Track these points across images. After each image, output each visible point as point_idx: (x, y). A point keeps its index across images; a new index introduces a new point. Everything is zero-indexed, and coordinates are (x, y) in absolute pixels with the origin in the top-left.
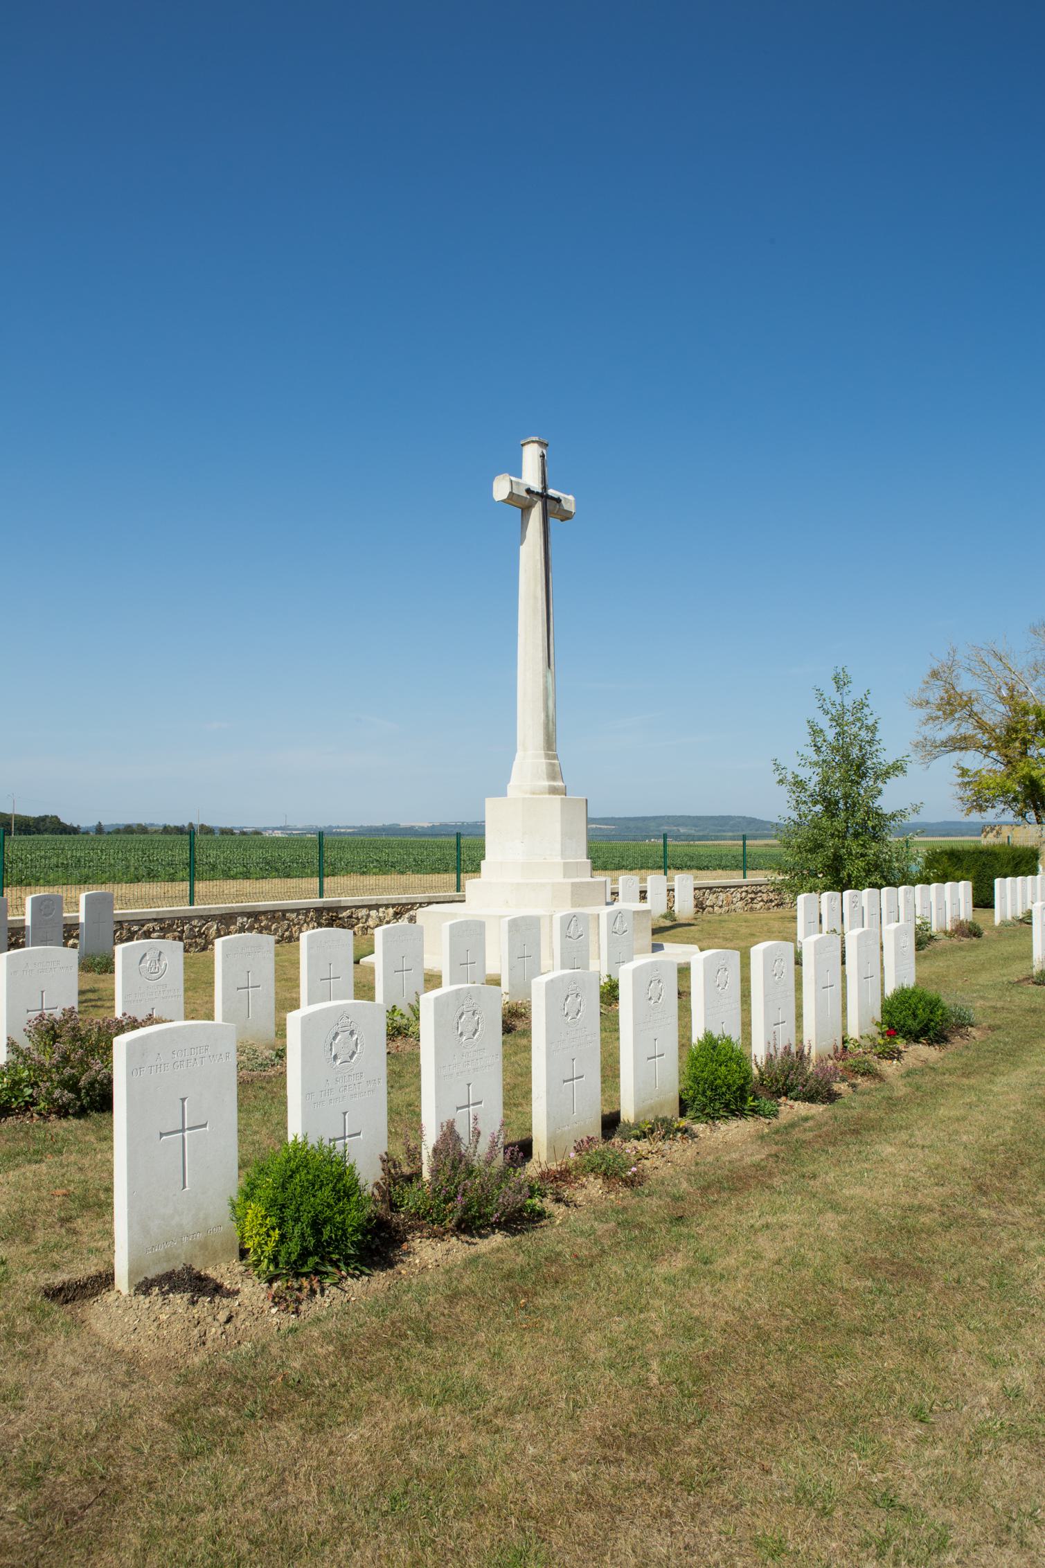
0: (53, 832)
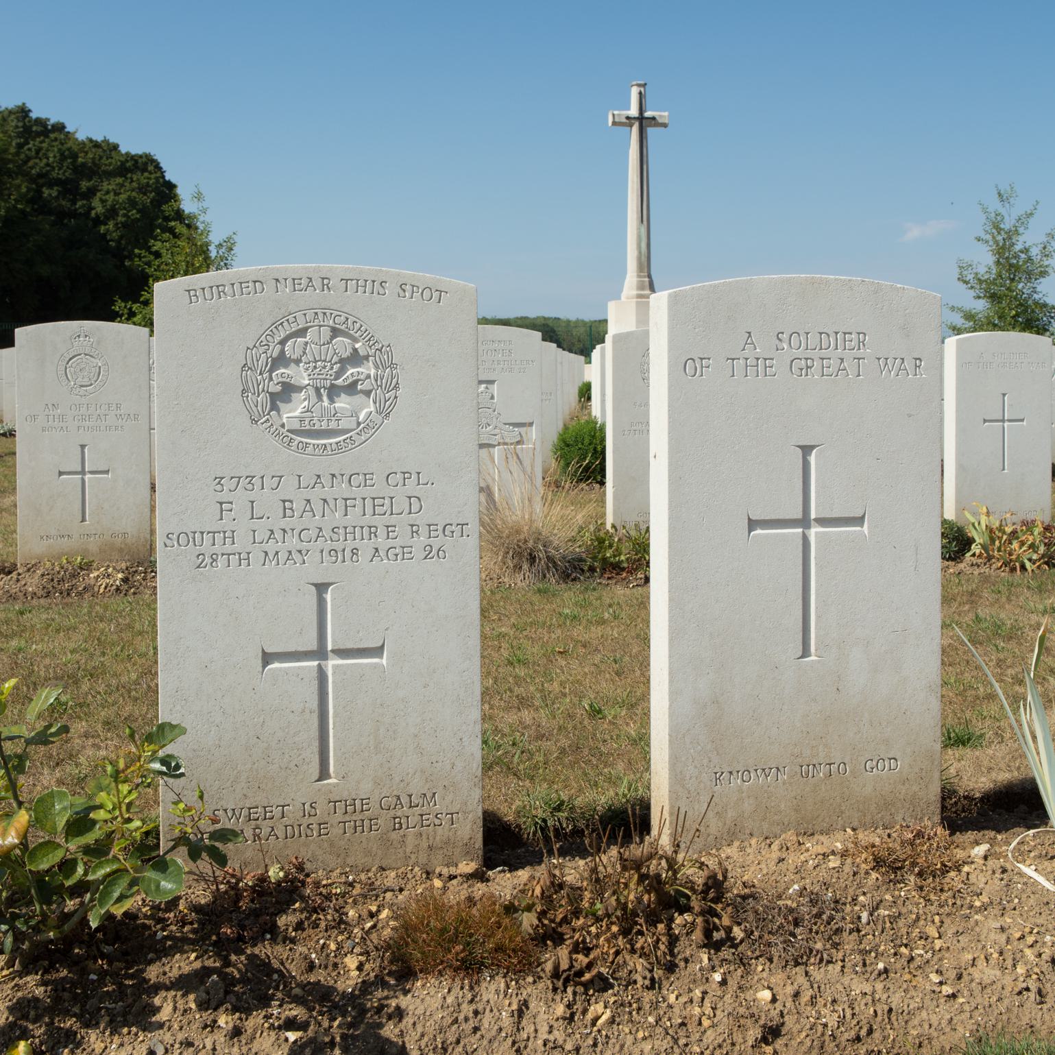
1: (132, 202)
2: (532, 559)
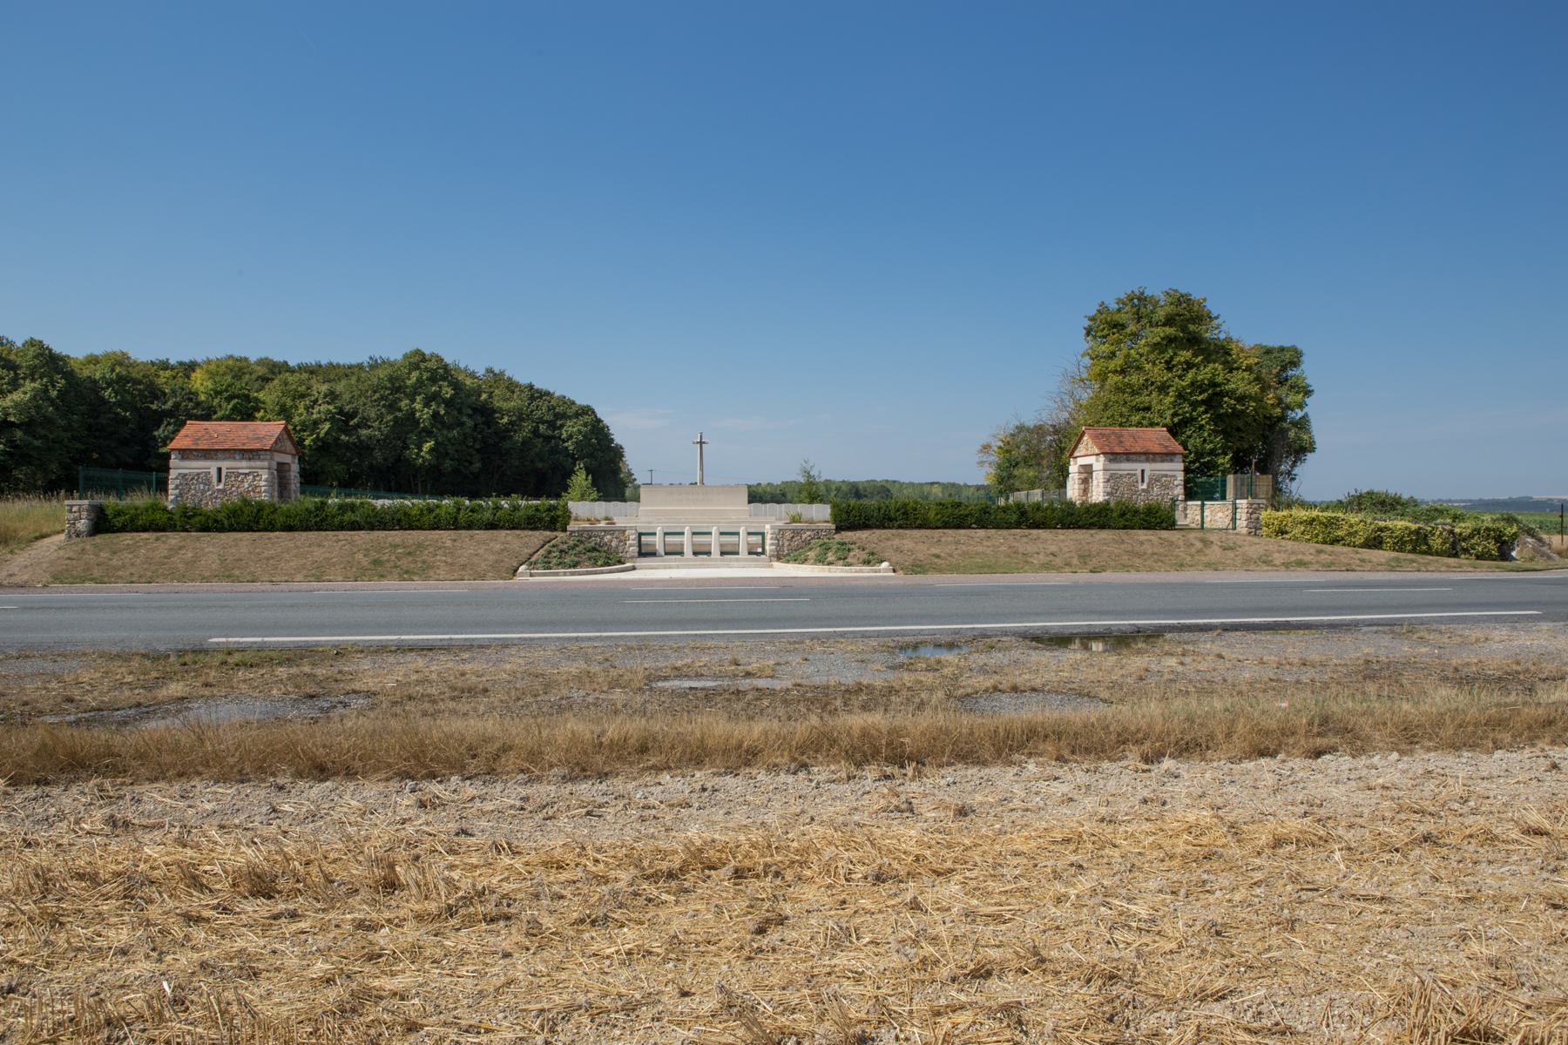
1: (580, 432)
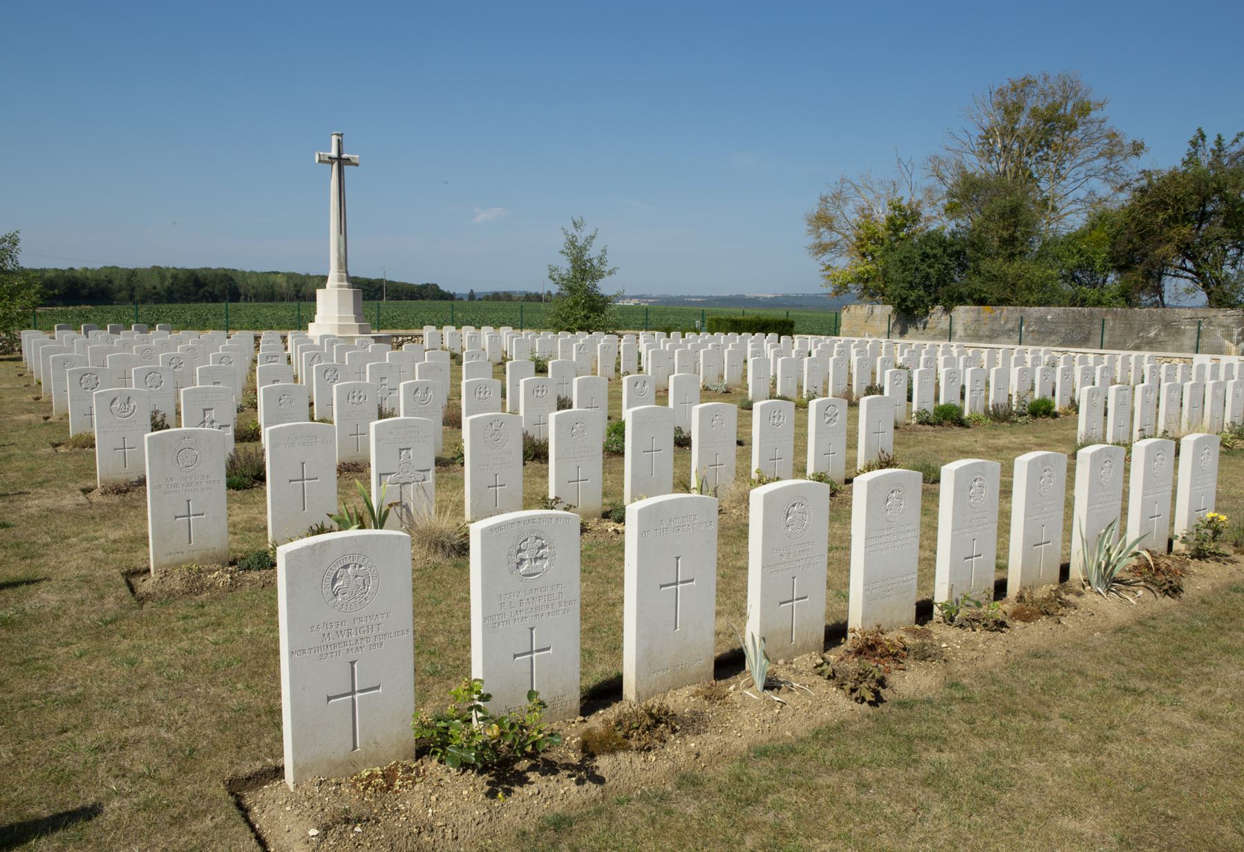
0: (434, 298)
2: (443, 547)
